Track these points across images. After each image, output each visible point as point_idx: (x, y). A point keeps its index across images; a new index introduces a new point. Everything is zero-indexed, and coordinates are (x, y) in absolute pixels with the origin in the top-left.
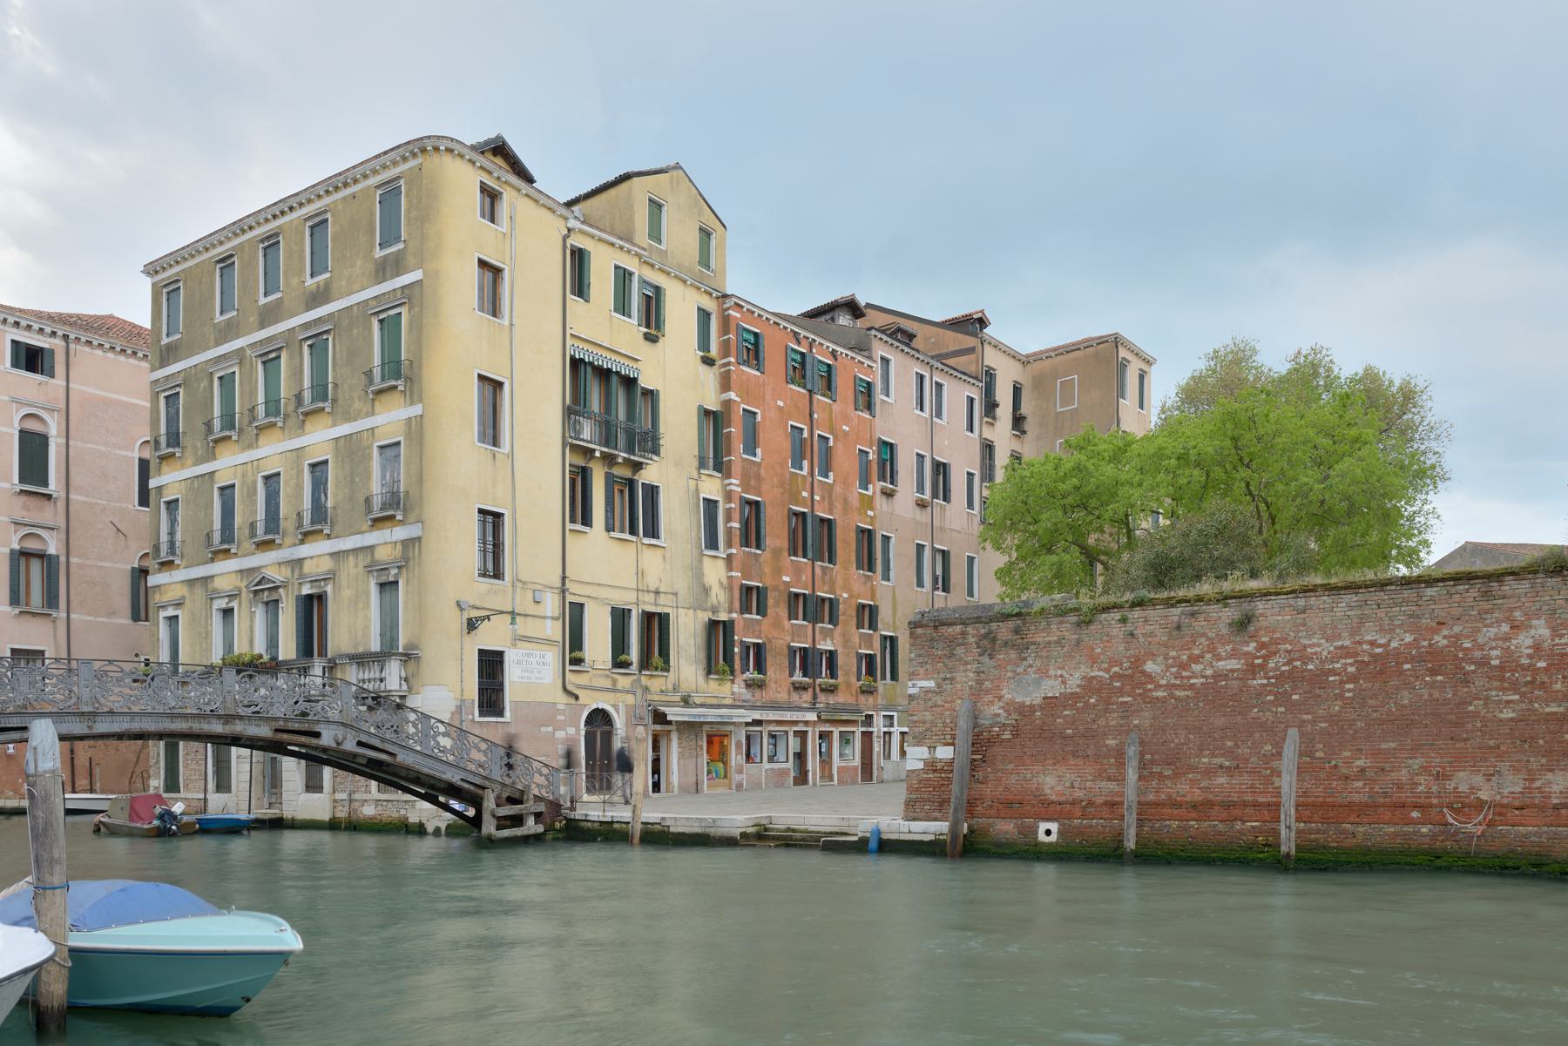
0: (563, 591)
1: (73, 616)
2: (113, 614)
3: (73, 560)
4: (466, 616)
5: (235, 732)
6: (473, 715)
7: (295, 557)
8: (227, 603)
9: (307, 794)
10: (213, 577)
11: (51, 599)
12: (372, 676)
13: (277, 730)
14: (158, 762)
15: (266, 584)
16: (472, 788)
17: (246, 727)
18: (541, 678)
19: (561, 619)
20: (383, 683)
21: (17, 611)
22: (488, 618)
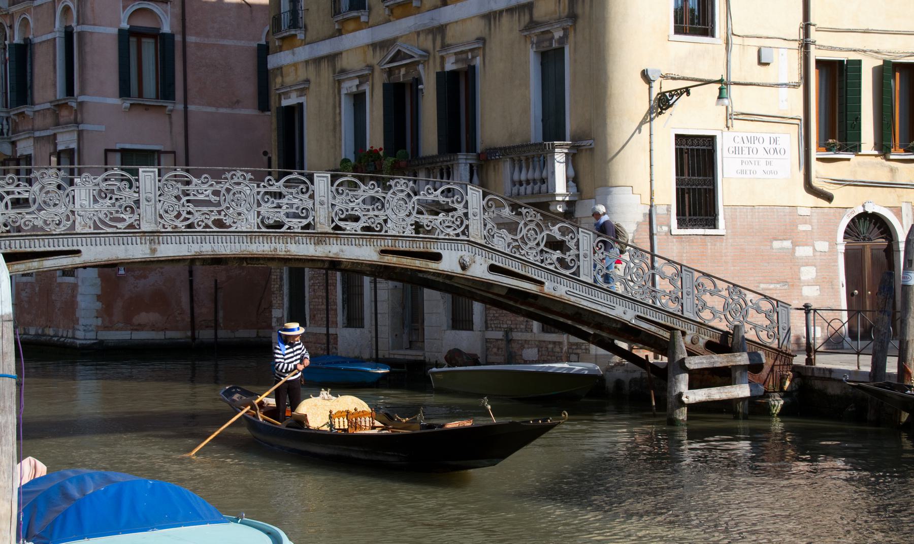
0: (805, 46)
1: (191, 108)
2: (237, 103)
3: (191, 39)
4: (656, 91)
5: (331, 255)
6: (670, 227)
7: (436, 23)
8: (358, 86)
9: (453, 332)
10: (341, 53)
11: (166, 91)
12: (530, 176)
13: (384, 252)
14: (281, 286)
15: (404, 59)
16: (653, 329)
17: (344, 247)
18: (771, 172)
19: (802, 86)
20: (545, 185)
21: (127, 104)
22: (687, 91)
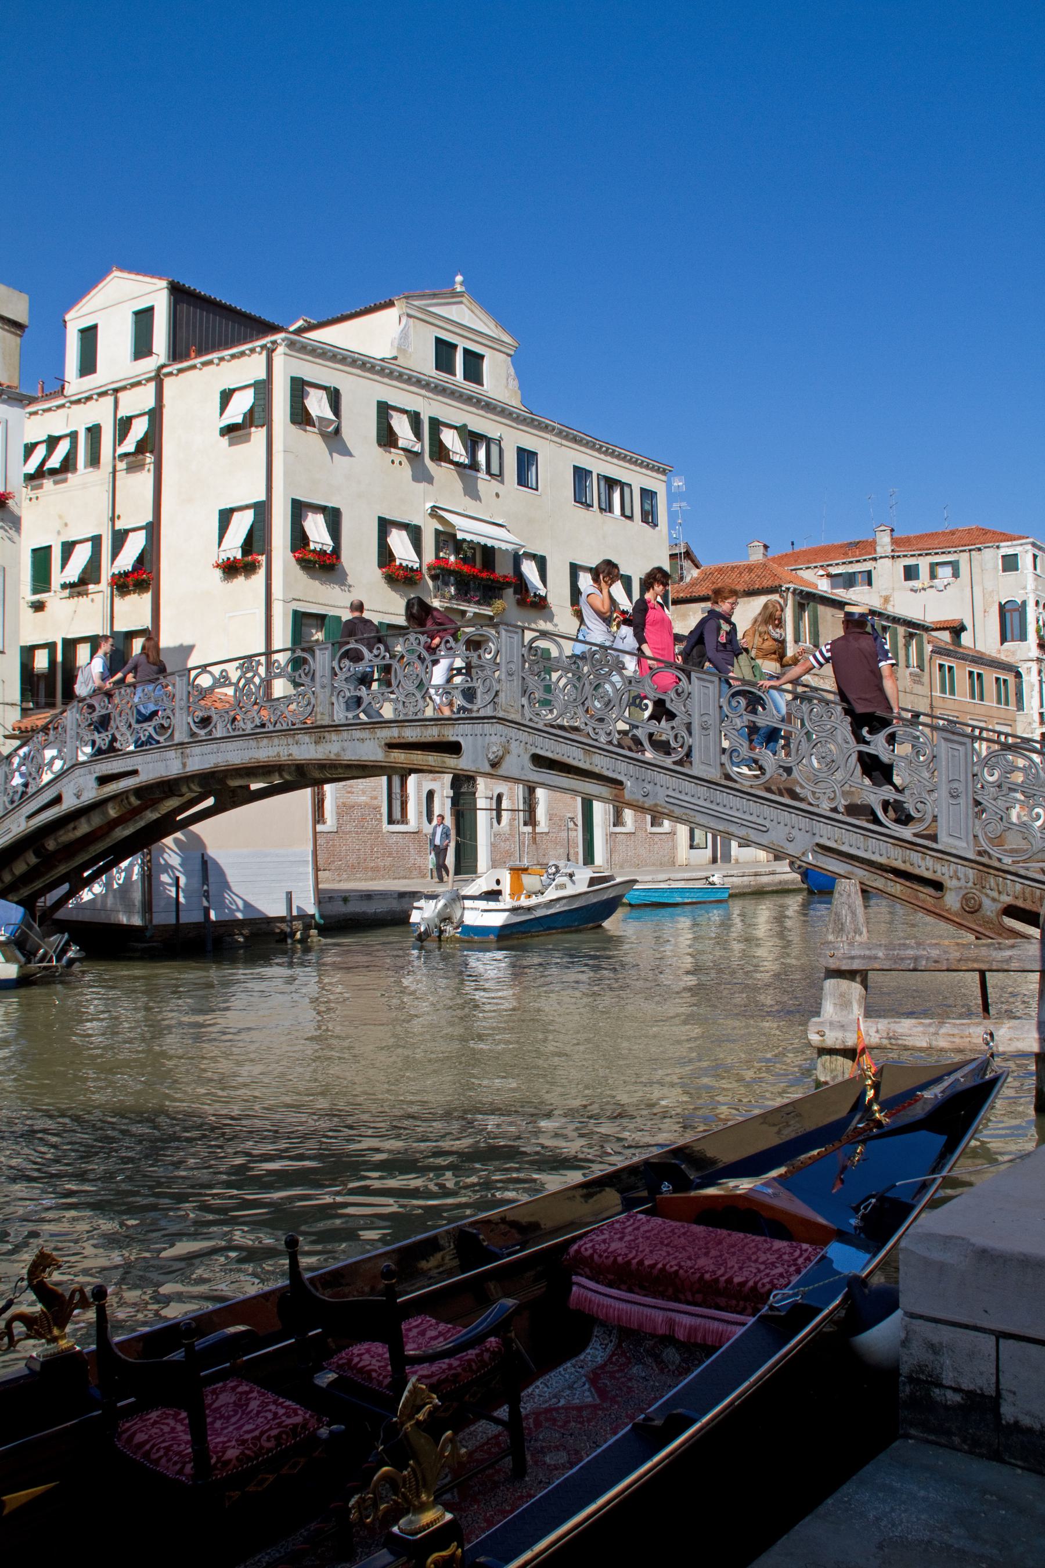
13: (391, 746)
